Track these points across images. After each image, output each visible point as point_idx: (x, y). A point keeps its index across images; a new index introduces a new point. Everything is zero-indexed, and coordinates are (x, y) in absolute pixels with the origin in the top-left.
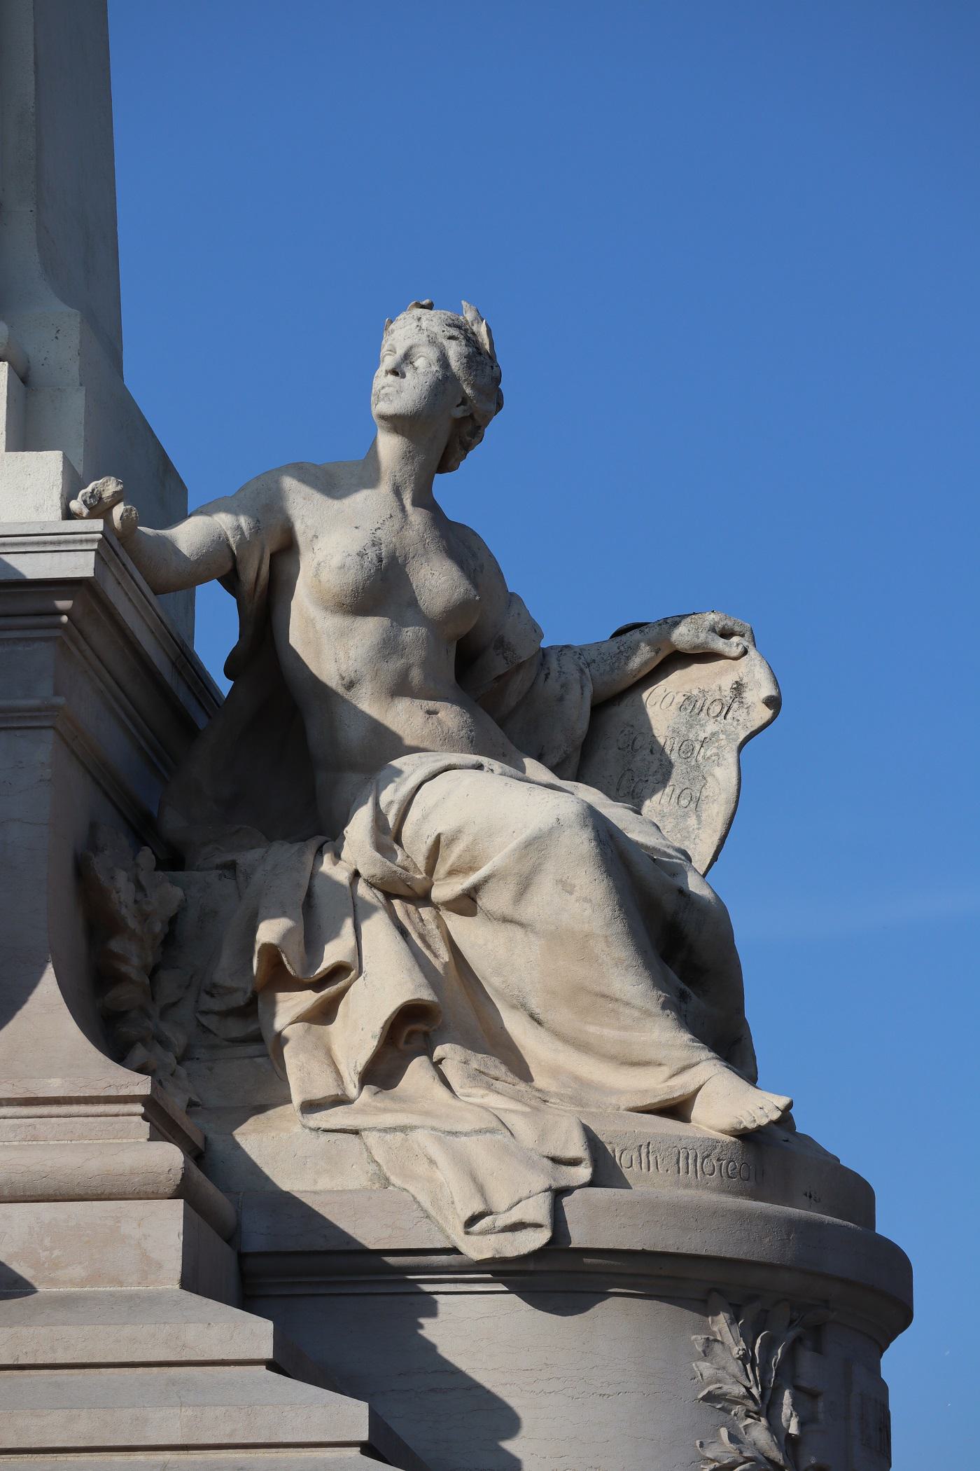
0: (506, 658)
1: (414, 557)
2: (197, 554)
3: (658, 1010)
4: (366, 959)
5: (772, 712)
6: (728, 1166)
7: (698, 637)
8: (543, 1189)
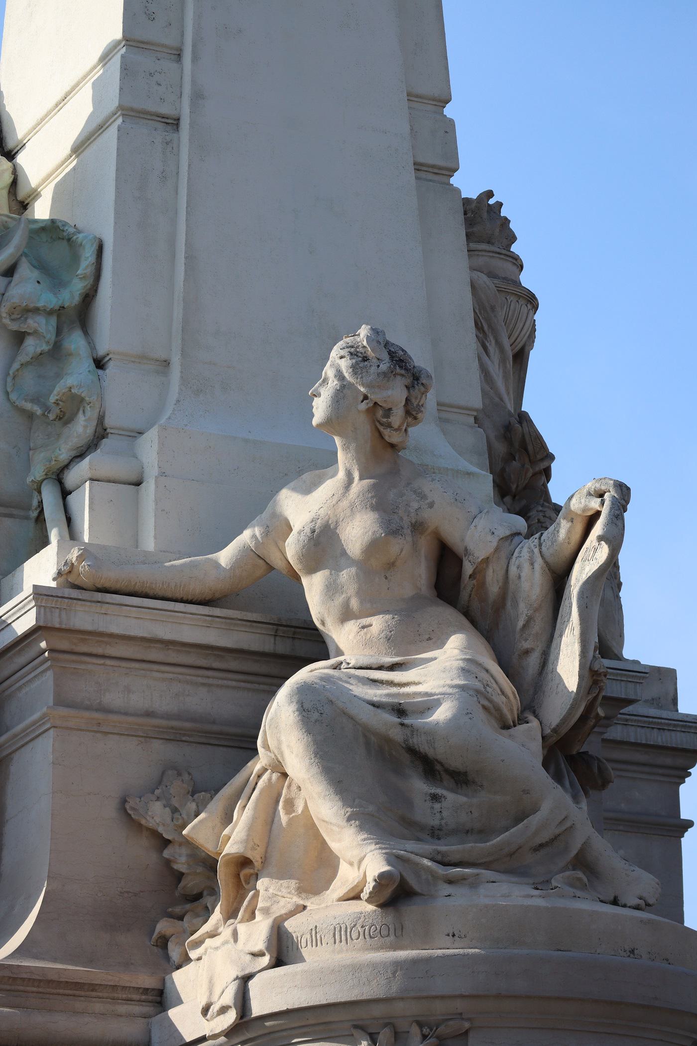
0: (470, 561)
1: (343, 520)
2: (230, 563)
3: (344, 823)
6: (370, 930)
7: (581, 503)
8: (233, 979)
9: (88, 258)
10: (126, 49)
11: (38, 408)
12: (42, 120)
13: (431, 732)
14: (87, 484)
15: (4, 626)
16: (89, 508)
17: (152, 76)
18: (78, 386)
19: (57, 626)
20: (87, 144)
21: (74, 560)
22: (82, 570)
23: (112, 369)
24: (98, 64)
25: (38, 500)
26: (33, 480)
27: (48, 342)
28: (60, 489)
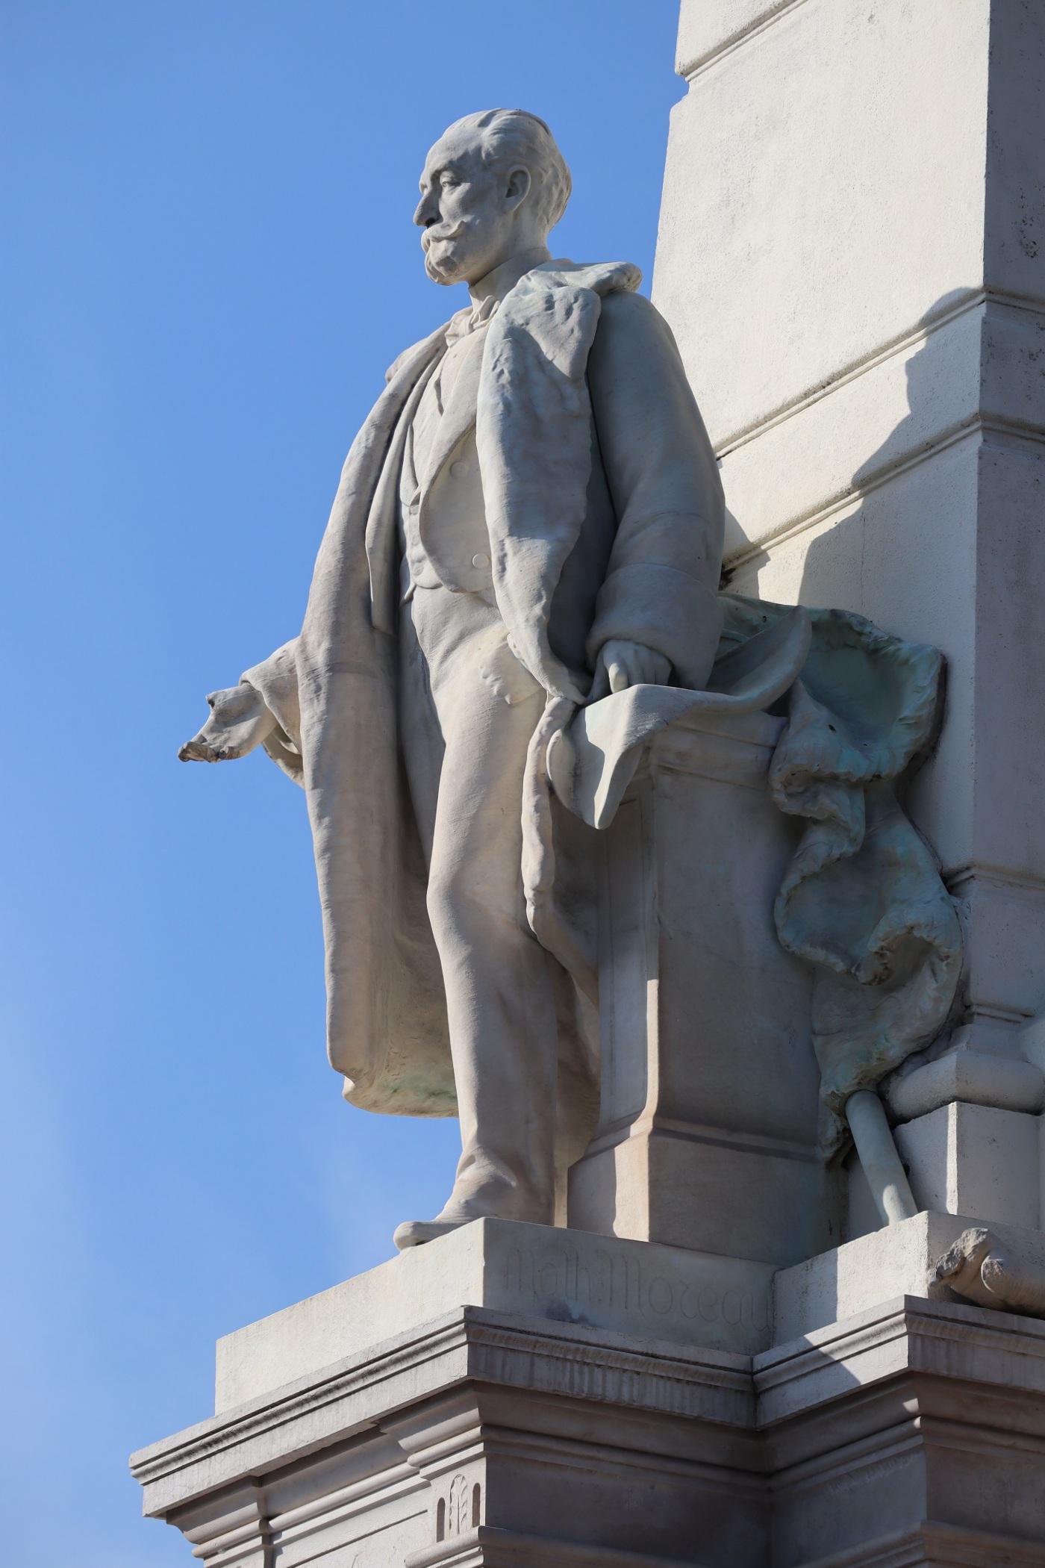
4: (864, 379)
5: (647, 1240)
9: (924, 688)
10: (987, 307)
11: (839, 960)
12: (768, 418)
14: (953, 1108)
15: (822, 1365)
16: (958, 1153)
17: (1035, 360)
18: (928, 925)
19: (944, 1372)
20: (892, 474)
21: (968, 1252)
22: (987, 1271)
23: (975, 894)
24: (916, 329)
25: (837, 1126)
26: (833, 1092)
27: (853, 841)
28: (883, 1115)
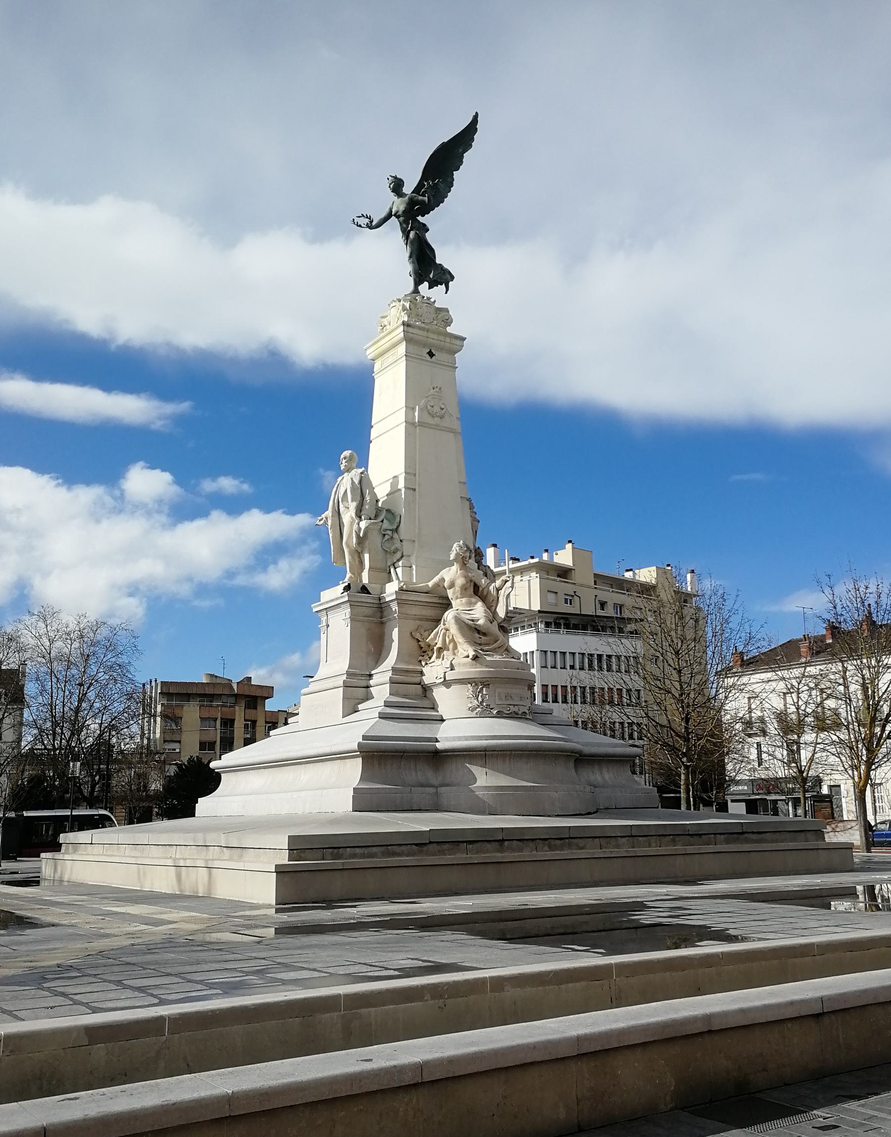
12: (381, 483)
13: (479, 625)
23: (404, 543)
